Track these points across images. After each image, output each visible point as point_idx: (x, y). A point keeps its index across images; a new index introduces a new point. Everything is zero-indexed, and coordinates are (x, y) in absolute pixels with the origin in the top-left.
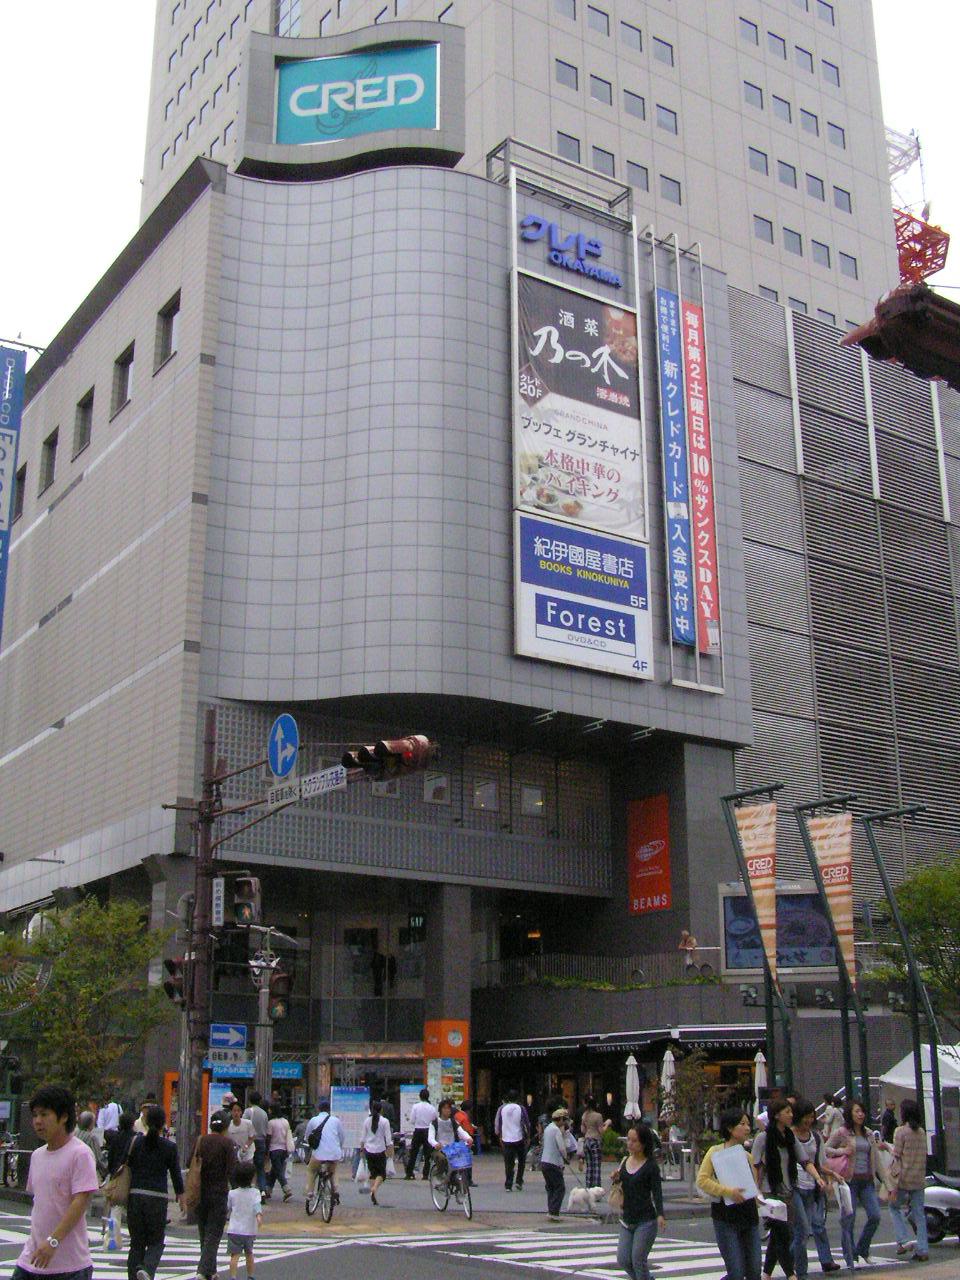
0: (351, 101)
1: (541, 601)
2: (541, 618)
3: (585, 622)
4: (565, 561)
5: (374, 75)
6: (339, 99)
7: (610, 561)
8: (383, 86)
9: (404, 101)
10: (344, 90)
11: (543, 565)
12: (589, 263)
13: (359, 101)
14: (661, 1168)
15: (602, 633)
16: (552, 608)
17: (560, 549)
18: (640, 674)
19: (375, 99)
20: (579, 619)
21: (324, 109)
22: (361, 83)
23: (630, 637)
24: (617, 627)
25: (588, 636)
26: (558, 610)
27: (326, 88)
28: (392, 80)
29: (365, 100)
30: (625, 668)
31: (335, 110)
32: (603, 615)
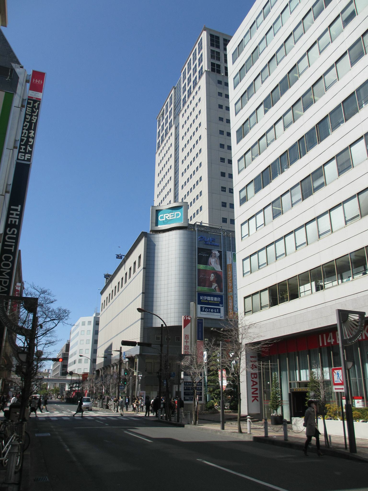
0: (169, 217)
1: (201, 308)
2: (201, 311)
3: (210, 310)
4: (206, 300)
5: (172, 212)
6: (167, 217)
7: (216, 299)
8: (174, 214)
9: (177, 217)
10: (167, 215)
11: (202, 301)
12: (213, 243)
13: (170, 217)
14: (11, 379)
15: (214, 312)
16: (204, 309)
17: (206, 298)
18: (221, 318)
19: (173, 217)
20: (209, 310)
21: (164, 219)
22: (170, 214)
23: (219, 312)
24: (217, 311)
25: (211, 313)
26: (205, 309)
27: (165, 215)
28: (176, 213)
29: (171, 217)
30: (218, 318)
31: (166, 219)
32: (214, 309)
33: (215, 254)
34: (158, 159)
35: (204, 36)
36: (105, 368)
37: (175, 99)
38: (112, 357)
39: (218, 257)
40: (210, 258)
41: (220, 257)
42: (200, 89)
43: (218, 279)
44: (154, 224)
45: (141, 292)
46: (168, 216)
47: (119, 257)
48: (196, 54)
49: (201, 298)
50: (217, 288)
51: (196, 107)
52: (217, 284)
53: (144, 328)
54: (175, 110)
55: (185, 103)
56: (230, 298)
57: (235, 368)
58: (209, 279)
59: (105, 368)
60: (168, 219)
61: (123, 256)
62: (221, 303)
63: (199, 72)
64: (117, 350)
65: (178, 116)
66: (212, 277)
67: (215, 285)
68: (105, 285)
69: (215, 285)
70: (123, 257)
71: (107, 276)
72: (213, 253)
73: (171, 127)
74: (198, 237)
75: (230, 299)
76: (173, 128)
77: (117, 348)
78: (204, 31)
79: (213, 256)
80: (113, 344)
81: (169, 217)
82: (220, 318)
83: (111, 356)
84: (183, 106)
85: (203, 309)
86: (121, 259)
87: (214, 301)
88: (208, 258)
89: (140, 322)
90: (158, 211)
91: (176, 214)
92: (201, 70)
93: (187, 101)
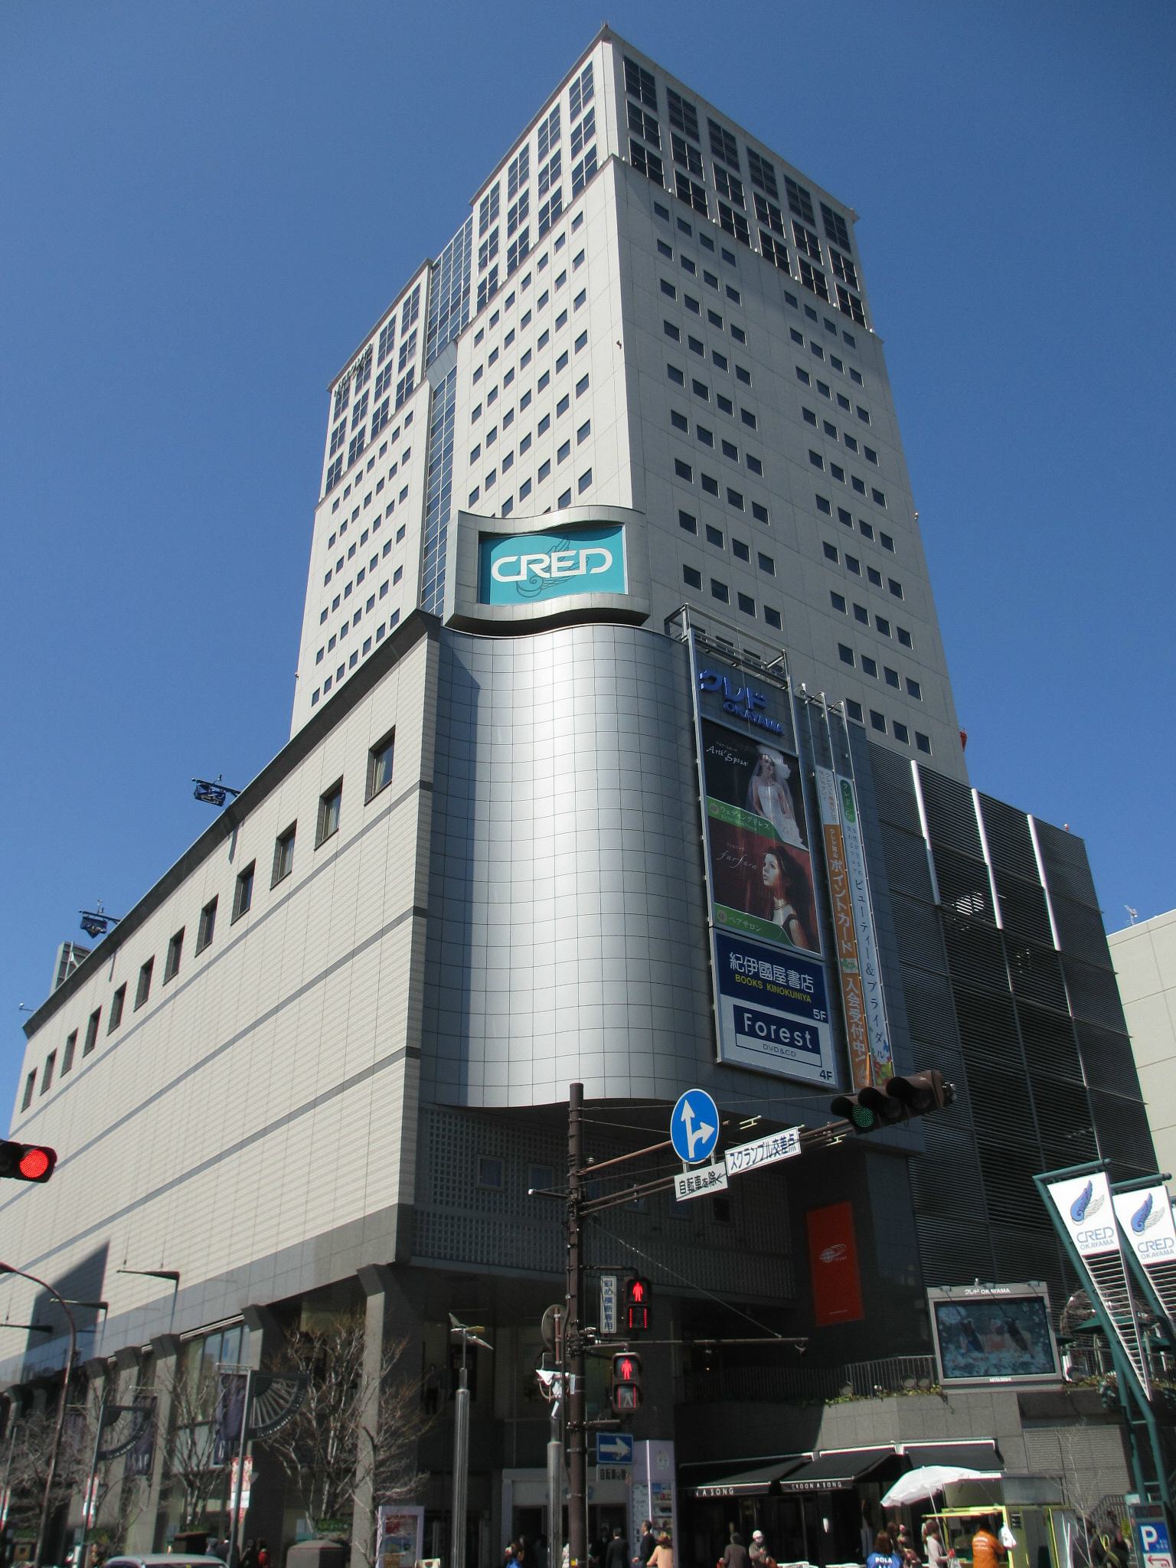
0: (548, 569)
1: (739, 1012)
5: (567, 549)
6: (537, 568)
8: (576, 558)
10: (541, 561)
13: (554, 569)
17: (753, 965)
19: (569, 569)
21: (523, 577)
22: (555, 556)
23: (816, 1049)
24: (804, 1038)
27: (524, 559)
28: (584, 553)
29: (560, 569)
30: (812, 1075)
31: (533, 577)
33: (773, 764)
34: (325, 521)
35: (602, 60)
36: (40, 1395)
37: (431, 302)
38: (101, 1319)
39: (786, 783)
40: (755, 779)
41: (793, 782)
42: (374, 469)
43: (794, 887)
44: (472, 594)
45: (409, 903)
46: (551, 562)
47: (205, 791)
48: (392, 334)
49: (734, 964)
50: (794, 924)
51: (403, 463)
52: (795, 909)
53: (421, 1110)
54: (429, 337)
55: (335, 476)
56: (851, 984)
57: (319, 1491)
58: (758, 877)
59: (40, 1395)
60: (547, 575)
61: (228, 795)
62: (818, 1001)
63: (353, 444)
64: (166, 1269)
65: (452, 343)
66: (772, 872)
67: (782, 913)
68: (53, 991)
69: (782, 913)
70: (230, 800)
71: (91, 924)
72: (767, 761)
73: (406, 391)
74: (697, 675)
75: (852, 990)
76: (419, 403)
77: (165, 1262)
78: (605, 40)
79: (766, 773)
80: (110, 1252)
81: (548, 569)
82: (822, 1079)
83: (96, 1317)
84: (329, 489)
85: (747, 1023)
86: (221, 804)
87: (788, 987)
88: (747, 774)
89: (398, 1070)
90: (489, 540)
91: (588, 558)
92: (491, 279)
93: (345, 473)
